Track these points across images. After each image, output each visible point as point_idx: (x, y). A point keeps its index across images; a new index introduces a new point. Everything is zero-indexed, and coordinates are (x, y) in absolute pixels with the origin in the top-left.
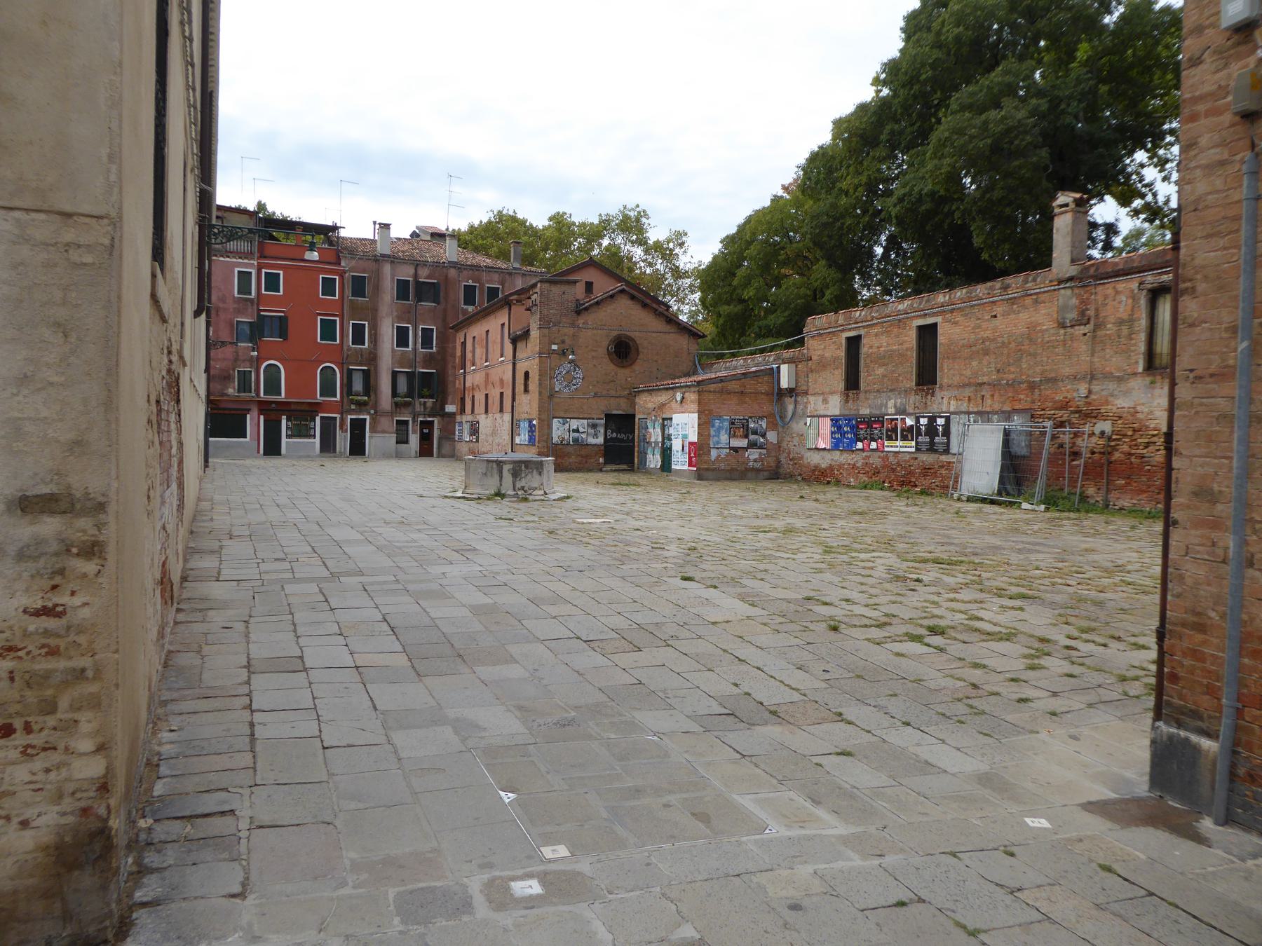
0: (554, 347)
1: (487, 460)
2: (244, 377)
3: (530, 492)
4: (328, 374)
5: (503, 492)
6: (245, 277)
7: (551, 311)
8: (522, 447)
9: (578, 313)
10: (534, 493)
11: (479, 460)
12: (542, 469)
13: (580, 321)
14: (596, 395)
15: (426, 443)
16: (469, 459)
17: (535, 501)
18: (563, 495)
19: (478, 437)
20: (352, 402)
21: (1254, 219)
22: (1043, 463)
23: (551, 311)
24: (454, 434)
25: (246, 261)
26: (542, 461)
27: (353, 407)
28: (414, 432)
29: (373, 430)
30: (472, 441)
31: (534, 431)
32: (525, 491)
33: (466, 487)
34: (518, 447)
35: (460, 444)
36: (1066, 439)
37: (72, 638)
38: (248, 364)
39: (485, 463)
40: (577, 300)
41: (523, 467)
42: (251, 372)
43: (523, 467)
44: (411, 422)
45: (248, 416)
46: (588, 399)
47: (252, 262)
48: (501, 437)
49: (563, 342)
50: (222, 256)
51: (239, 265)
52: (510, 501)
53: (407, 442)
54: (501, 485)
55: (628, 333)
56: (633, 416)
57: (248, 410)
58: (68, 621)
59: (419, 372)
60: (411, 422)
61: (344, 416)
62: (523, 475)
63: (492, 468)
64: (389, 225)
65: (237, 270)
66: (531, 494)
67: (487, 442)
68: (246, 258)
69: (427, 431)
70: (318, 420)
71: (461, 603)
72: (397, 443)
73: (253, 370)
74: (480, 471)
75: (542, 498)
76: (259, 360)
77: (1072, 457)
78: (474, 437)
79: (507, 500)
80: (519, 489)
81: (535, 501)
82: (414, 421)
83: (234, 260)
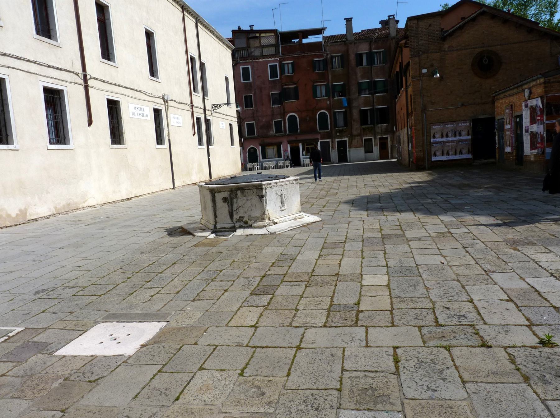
0: (424, 71)
2: (278, 124)
4: (322, 116)
6: (273, 68)
7: (420, 43)
9: (444, 39)
13: (446, 46)
14: (463, 105)
20: (337, 132)
21: (231, 417)
22: (367, 126)
23: (420, 43)
25: (273, 59)
27: (338, 134)
28: (376, 145)
29: (350, 147)
38: (279, 117)
40: (442, 30)
42: (281, 121)
44: (373, 139)
45: (281, 145)
46: (456, 109)
47: (276, 59)
49: (432, 66)
50: (261, 59)
51: (270, 62)
53: (372, 151)
55: (490, 48)
56: (494, 118)
57: (281, 143)
59: (376, 108)
60: (373, 139)
61: (334, 140)
64: (351, 18)
65: (269, 65)
68: (270, 58)
70: (319, 143)
71: (242, 307)
72: (366, 152)
73: (282, 120)
76: (283, 115)
82: (375, 138)
83: (267, 59)
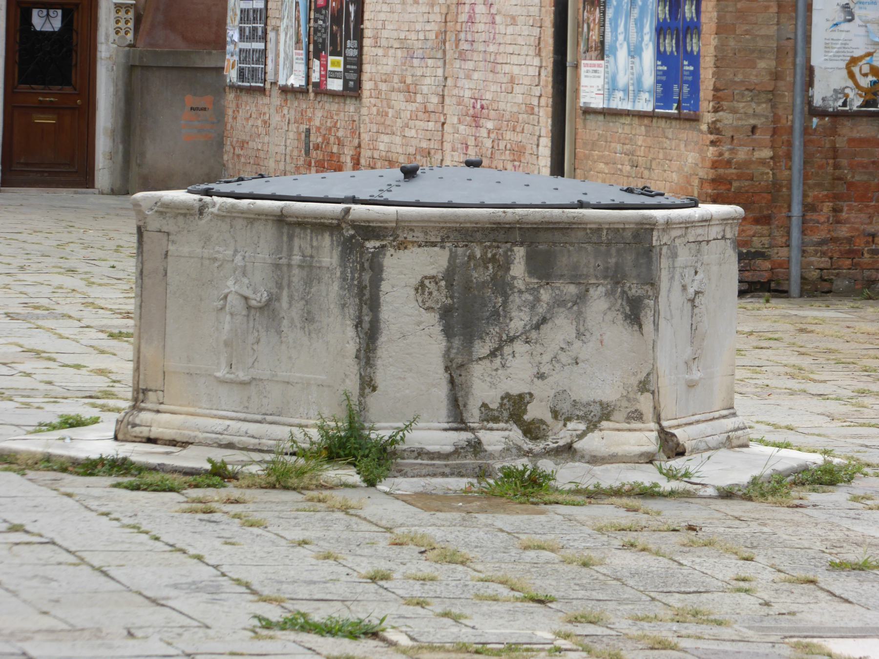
1: (281, 220)
3: (562, 435)
5: (381, 432)
8: (621, 127)
10: (593, 443)
11: (228, 215)
12: (652, 283)
15: (49, 95)
16: (166, 210)
17: (595, 495)
18: (791, 458)
19: (356, 65)
24: (219, 43)
26: (646, 229)
30: (320, 89)
31: (693, 28)
32: (532, 431)
33: (140, 395)
34: (595, 128)
35: (250, 105)
36: (308, 289)
37: (834, 613)
39: (267, 233)
41: (518, 269)
43: (518, 269)
48: (494, 66)
52: (410, 500)
54: (368, 384)
58: (602, 612)
62: (518, 321)
63: (309, 266)
66: (568, 451)
67: (410, 92)
69: (56, 23)
74: (231, 285)
75: (646, 476)
77: (251, 69)
78: (336, 63)
79: (406, 485)
80: (490, 416)
81: (595, 495)
